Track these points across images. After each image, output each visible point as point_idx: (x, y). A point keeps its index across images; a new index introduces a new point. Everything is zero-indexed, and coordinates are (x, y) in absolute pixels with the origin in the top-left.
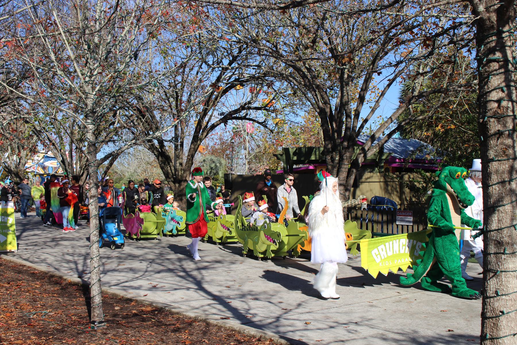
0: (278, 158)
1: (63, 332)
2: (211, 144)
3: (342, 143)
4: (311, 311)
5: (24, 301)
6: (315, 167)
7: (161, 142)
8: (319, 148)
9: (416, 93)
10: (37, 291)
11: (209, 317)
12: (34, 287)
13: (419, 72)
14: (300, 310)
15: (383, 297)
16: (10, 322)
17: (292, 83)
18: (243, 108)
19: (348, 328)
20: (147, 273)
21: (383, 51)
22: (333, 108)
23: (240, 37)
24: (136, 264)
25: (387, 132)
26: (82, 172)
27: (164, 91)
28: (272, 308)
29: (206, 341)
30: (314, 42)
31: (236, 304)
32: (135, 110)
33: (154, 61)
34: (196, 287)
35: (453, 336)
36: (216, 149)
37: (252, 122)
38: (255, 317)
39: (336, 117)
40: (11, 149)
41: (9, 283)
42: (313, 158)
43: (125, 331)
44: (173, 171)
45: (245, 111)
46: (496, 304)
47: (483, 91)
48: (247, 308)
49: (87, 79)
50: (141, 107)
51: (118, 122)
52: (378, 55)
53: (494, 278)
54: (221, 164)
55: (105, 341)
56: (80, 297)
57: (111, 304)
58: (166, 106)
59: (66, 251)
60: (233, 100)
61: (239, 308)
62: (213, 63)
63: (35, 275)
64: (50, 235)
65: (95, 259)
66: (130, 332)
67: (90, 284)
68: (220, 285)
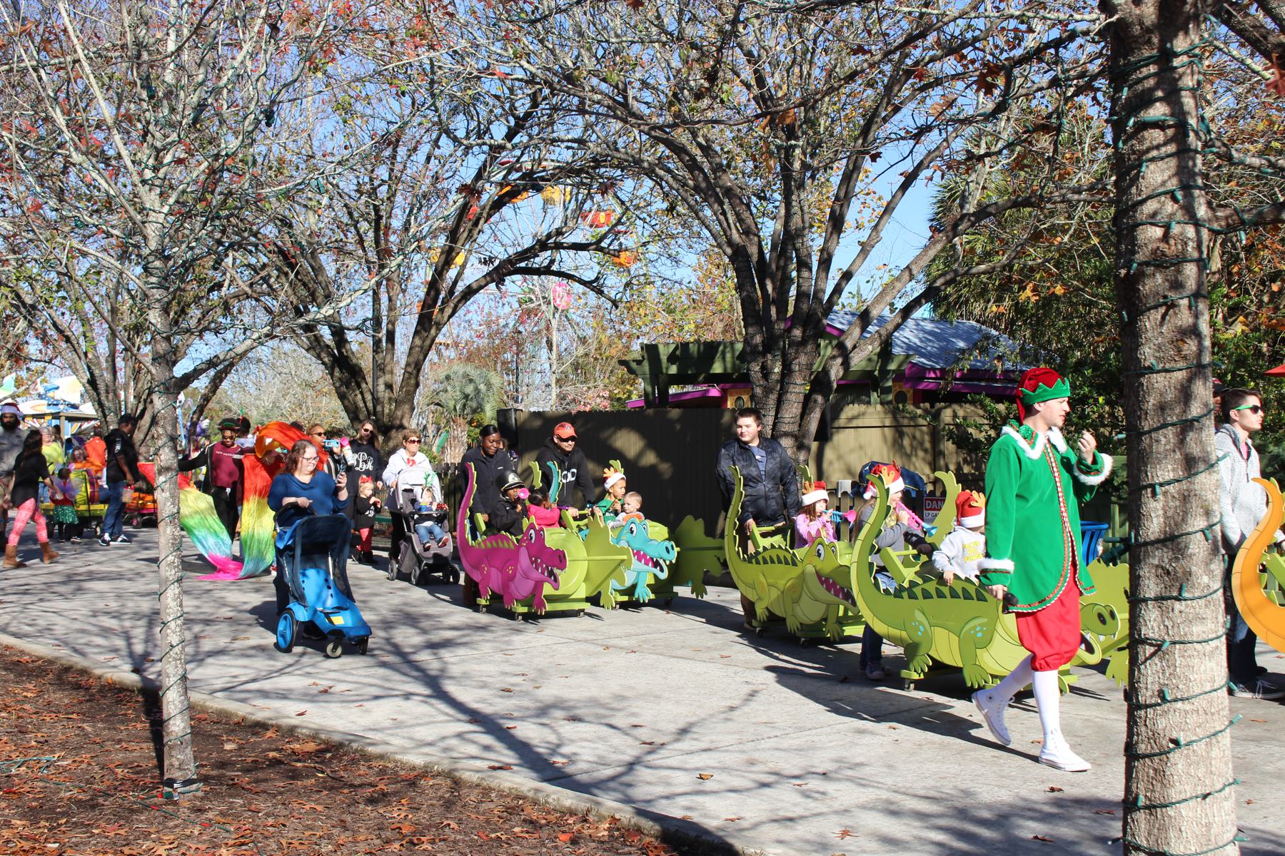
0: (631, 371)
1: (93, 807)
4: (712, 746)
7: (339, 333)
8: (732, 344)
9: (971, 208)
10: (27, 706)
12: (20, 698)
18: (542, 245)
23: (533, 69)
26: (141, 407)
28: (617, 739)
29: (453, 825)
31: (527, 731)
34: (427, 691)
35: (1058, 803)
39: (774, 266)
42: (717, 368)
43: (250, 804)
44: (370, 405)
45: (549, 252)
46: (1162, 723)
47: (1128, 200)
49: (148, 174)
50: (287, 243)
52: (875, 113)
53: (1156, 659)
54: (489, 385)
55: (198, 828)
56: (137, 719)
57: (215, 736)
59: (100, 605)
60: (524, 222)
61: (535, 742)
62: (468, 133)
65: (172, 625)
66: (263, 805)
68: (484, 686)
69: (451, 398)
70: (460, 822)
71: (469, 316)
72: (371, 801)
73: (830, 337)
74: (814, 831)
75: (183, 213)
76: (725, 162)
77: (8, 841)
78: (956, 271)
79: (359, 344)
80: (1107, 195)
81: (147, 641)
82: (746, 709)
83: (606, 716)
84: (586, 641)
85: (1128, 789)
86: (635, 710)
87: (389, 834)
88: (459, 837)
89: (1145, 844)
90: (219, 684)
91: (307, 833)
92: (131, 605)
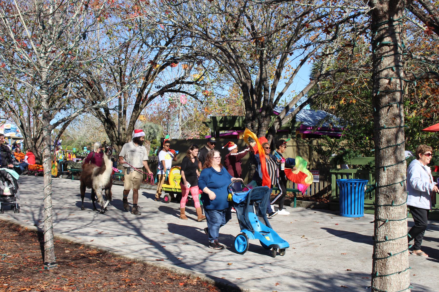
1: (20, 272)
2: (150, 113)
7: (107, 111)
9: (323, 72)
15: (294, 242)
18: (177, 82)
20: (94, 222)
22: (254, 84)
23: (175, 22)
26: (38, 135)
29: (143, 279)
34: (136, 234)
35: (350, 274)
36: (154, 117)
37: (185, 94)
38: (185, 258)
43: (74, 271)
45: (179, 85)
46: (385, 248)
49: (42, 55)
53: (384, 226)
54: (158, 130)
57: (62, 248)
60: (169, 75)
61: (172, 251)
62: (152, 43)
65: (48, 210)
66: (78, 272)
68: (155, 232)
70: (146, 278)
71: (152, 106)
75: (54, 69)
81: (39, 216)
88: (145, 283)
89: (379, 288)
91: (93, 282)
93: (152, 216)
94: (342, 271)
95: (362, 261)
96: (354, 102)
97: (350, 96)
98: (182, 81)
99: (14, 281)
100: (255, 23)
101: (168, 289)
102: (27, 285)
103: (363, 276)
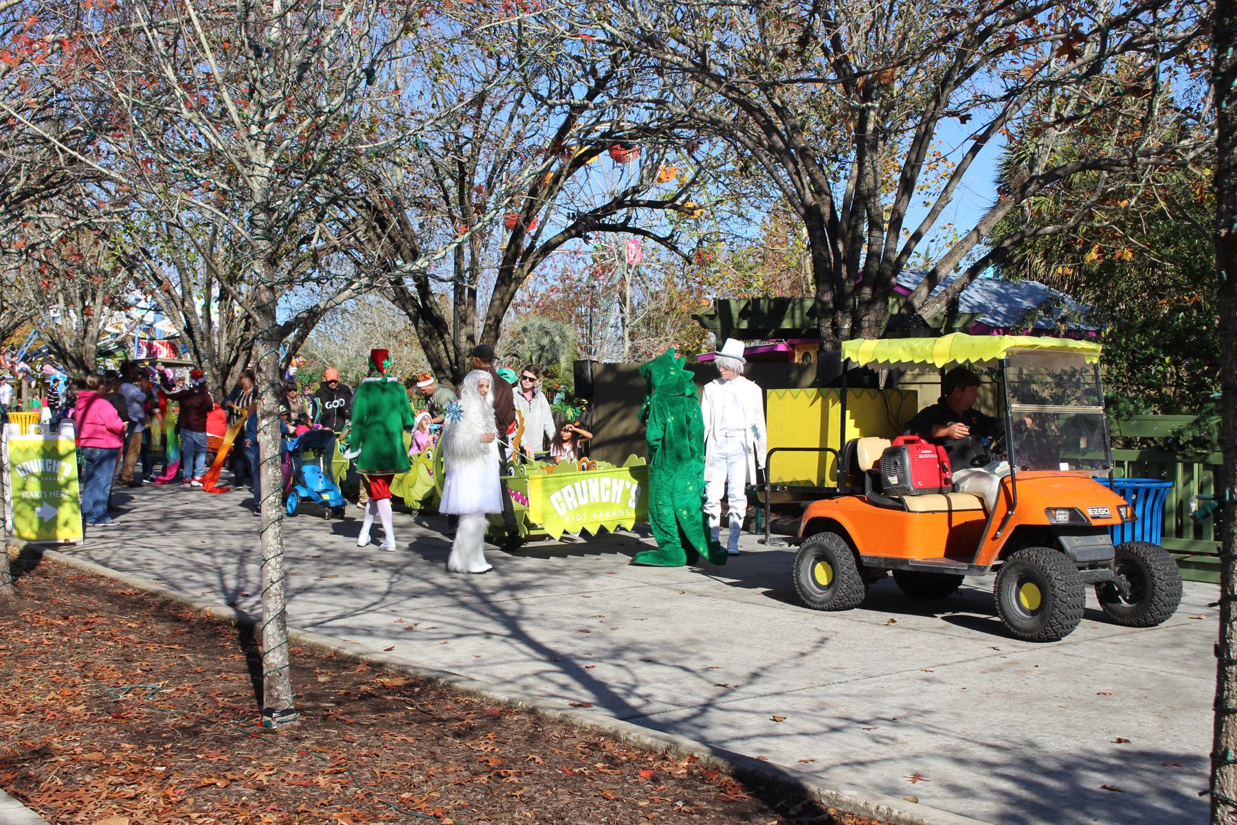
0: (703, 325)
1: (196, 734)
2: (542, 290)
3: (858, 288)
4: (784, 689)
5: (102, 661)
6: (792, 346)
7: (423, 283)
8: (802, 300)
9: (1039, 171)
10: (132, 637)
11: (540, 703)
12: (125, 628)
13: (1061, 115)
14: (758, 688)
15: (959, 658)
16: (71, 709)
17: (739, 144)
18: (618, 203)
19: (873, 732)
20: (389, 598)
21: (960, 72)
22: (839, 204)
23: (615, 32)
24: (361, 576)
25: (965, 265)
26: (234, 354)
27: (433, 163)
28: (690, 681)
29: (538, 759)
30: (803, 42)
31: (604, 672)
32: (361, 207)
33: (410, 89)
34: (507, 632)
35: (1123, 755)
36: (553, 302)
37: (641, 237)
38: (648, 702)
39: (845, 226)
40: (65, 300)
41: (66, 618)
42: (786, 324)
43: (345, 734)
44: (452, 355)
45: (625, 210)
47: (1230, 160)
48: (632, 682)
49: (254, 130)
50: (374, 198)
51: (320, 237)
52: (948, 76)
54: (564, 337)
55: (296, 755)
56: (235, 651)
57: (309, 668)
58: (433, 193)
59: (196, 542)
60: (599, 181)
61: (612, 682)
62: (550, 93)
63: (139, 602)
64: (158, 505)
65: (273, 562)
66: (357, 736)
67: (261, 620)
68: (560, 627)
69: (527, 349)
71: (545, 271)
72: (457, 735)
73: (898, 296)
74: (886, 774)
75: (282, 169)
76: (798, 123)
77: (118, 764)
78: (1022, 232)
79: (443, 293)
80: (1175, 159)
81: (238, 577)
82: (817, 655)
83: (679, 660)
84: (660, 585)
85: (1217, 743)
86: (705, 653)
87: (476, 766)
88: (544, 771)
90: (307, 620)
91: (400, 764)
92: (223, 543)
93: (547, 582)
94: (1101, 745)
95: (1160, 715)
96: (1129, 256)
97: (1115, 238)
98: (631, 200)
99: (183, 760)
100: (843, 30)
101: (609, 786)
102: (219, 771)
103: (1187, 762)
